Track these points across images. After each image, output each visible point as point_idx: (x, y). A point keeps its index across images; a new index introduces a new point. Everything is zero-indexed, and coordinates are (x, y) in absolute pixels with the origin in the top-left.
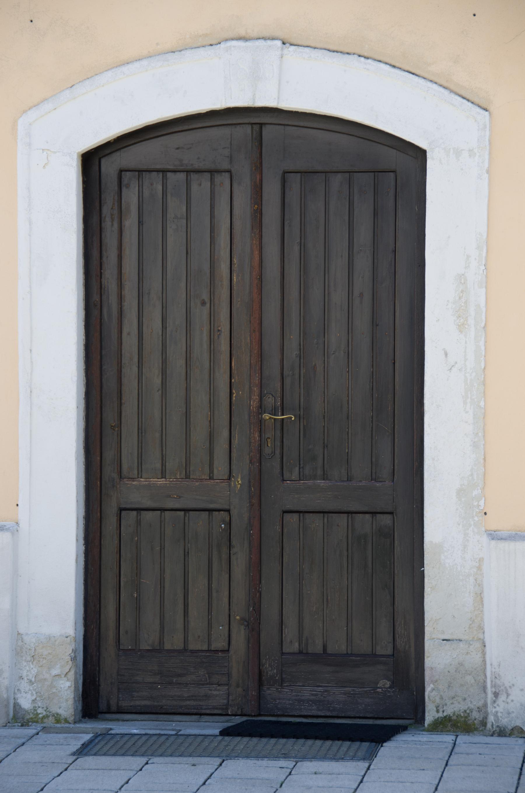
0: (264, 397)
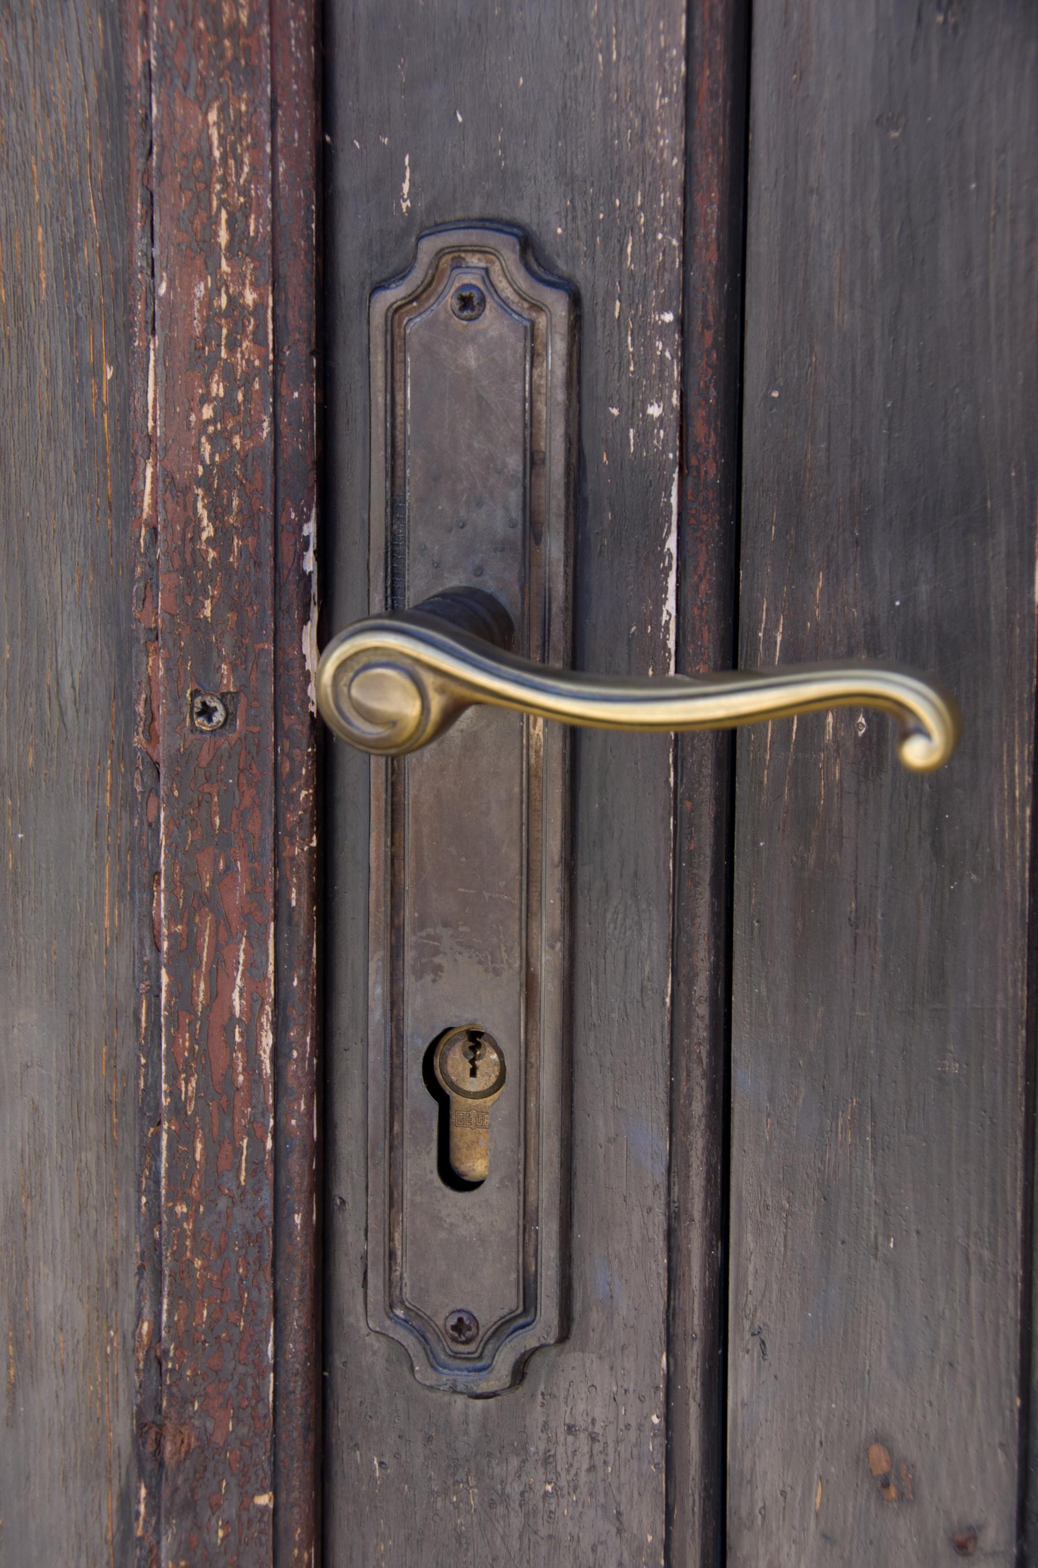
0: (379, 286)
